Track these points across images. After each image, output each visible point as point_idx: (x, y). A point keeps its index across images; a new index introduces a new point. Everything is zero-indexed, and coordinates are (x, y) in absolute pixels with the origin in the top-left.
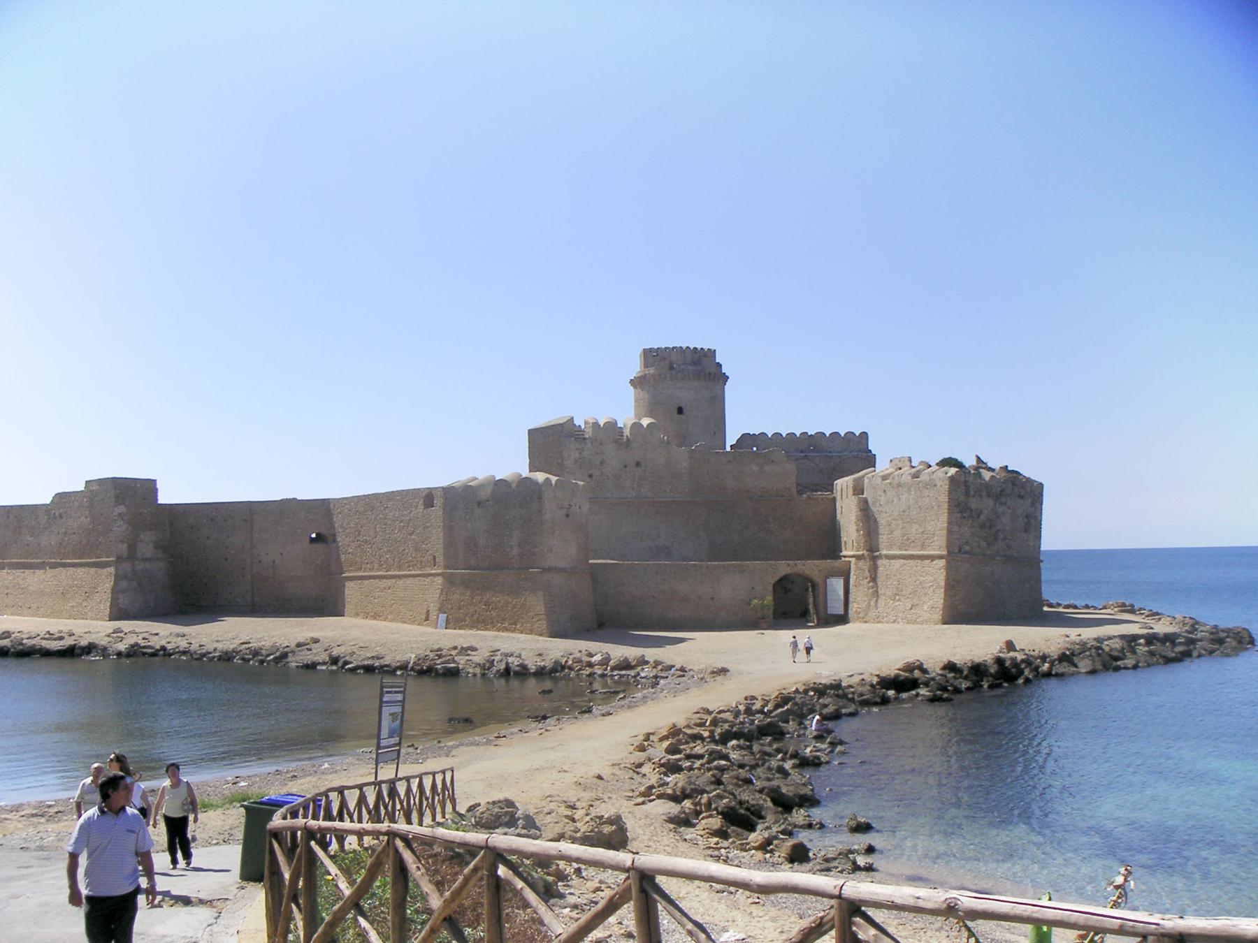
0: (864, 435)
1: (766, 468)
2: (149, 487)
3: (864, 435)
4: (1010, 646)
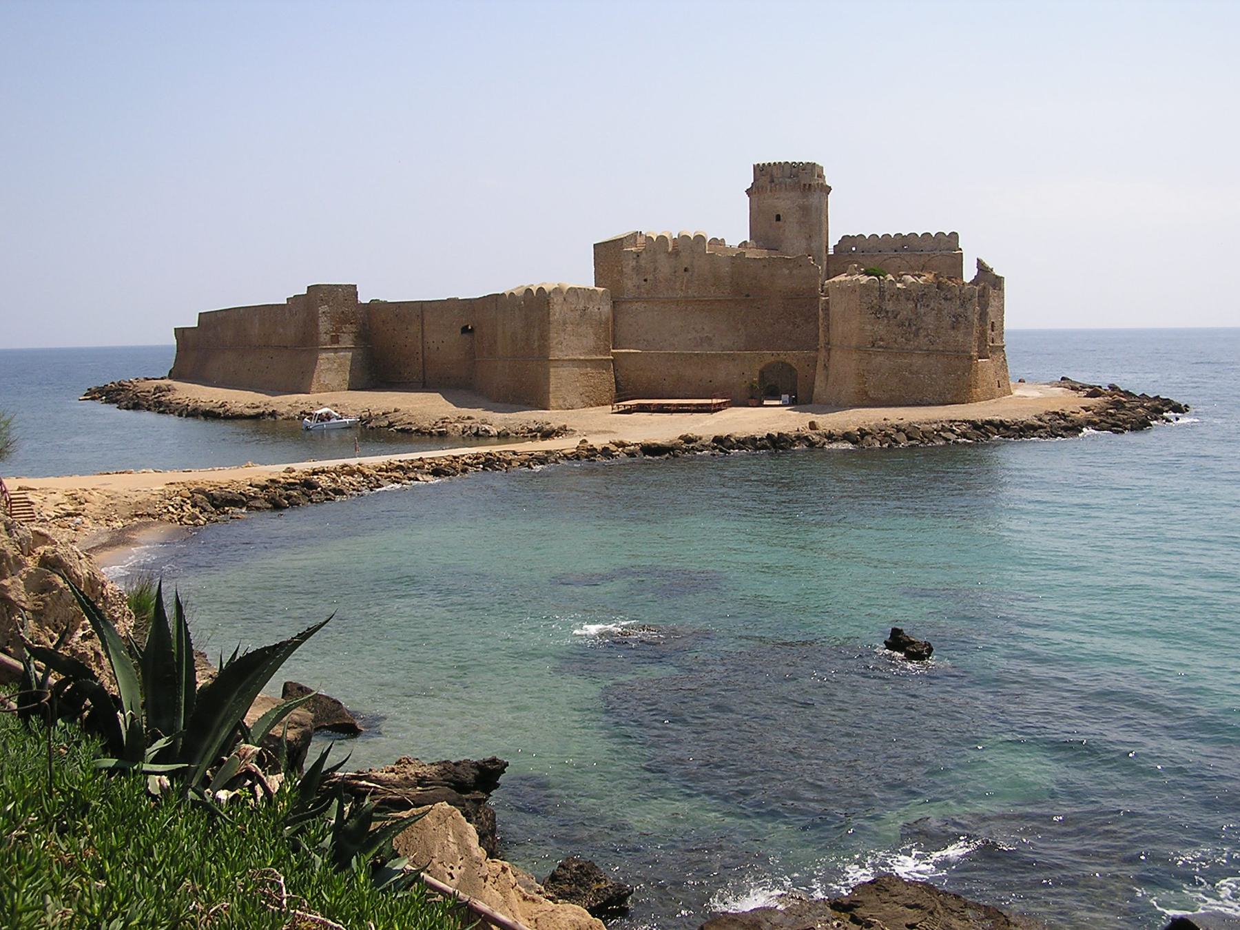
0: (954, 235)
1: (795, 272)
2: (352, 290)
3: (954, 235)
4: (812, 426)
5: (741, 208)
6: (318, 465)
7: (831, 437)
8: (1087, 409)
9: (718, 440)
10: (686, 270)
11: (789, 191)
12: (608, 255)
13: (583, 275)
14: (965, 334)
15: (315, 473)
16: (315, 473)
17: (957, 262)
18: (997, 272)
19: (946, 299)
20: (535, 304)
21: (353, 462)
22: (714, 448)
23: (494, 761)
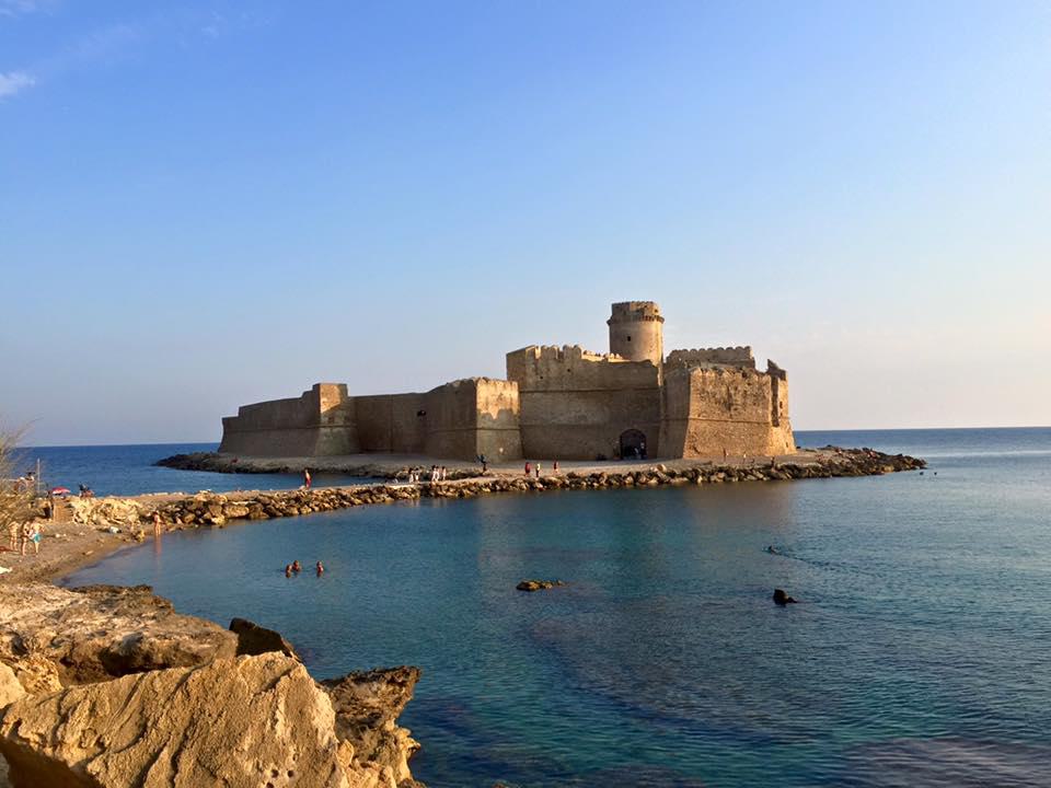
19: (749, 384)
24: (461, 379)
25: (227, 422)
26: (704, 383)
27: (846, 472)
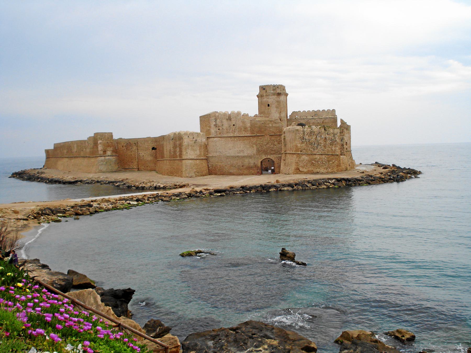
0: (334, 111)
2: (111, 135)
4: (277, 181)
5: (256, 101)
6: (94, 199)
7: (284, 186)
8: (381, 173)
9: (243, 187)
10: (234, 125)
11: (272, 95)
12: (205, 120)
13: (196, 128)
14: (335, 147)
15: (92, 201)
16: (92, 201)
17: (335, 120)
18: (348, 124)
19: (328, 134)
20: (177, 139)
21: (107, 197)
22: (241, 190)
23: (129, 289)
24: (174, 132)
25: (47, 152)
26: (304, 134)
27: (382, 180)
